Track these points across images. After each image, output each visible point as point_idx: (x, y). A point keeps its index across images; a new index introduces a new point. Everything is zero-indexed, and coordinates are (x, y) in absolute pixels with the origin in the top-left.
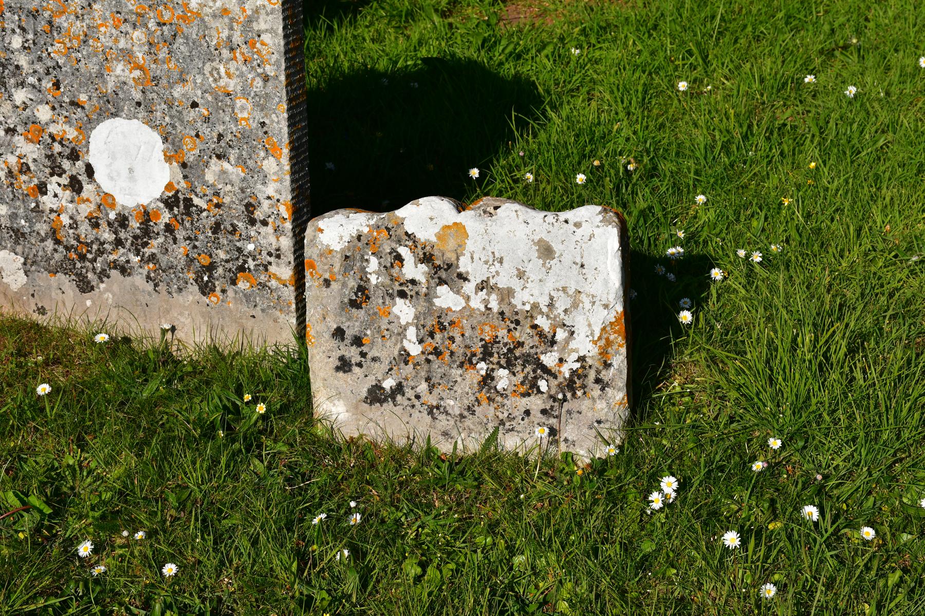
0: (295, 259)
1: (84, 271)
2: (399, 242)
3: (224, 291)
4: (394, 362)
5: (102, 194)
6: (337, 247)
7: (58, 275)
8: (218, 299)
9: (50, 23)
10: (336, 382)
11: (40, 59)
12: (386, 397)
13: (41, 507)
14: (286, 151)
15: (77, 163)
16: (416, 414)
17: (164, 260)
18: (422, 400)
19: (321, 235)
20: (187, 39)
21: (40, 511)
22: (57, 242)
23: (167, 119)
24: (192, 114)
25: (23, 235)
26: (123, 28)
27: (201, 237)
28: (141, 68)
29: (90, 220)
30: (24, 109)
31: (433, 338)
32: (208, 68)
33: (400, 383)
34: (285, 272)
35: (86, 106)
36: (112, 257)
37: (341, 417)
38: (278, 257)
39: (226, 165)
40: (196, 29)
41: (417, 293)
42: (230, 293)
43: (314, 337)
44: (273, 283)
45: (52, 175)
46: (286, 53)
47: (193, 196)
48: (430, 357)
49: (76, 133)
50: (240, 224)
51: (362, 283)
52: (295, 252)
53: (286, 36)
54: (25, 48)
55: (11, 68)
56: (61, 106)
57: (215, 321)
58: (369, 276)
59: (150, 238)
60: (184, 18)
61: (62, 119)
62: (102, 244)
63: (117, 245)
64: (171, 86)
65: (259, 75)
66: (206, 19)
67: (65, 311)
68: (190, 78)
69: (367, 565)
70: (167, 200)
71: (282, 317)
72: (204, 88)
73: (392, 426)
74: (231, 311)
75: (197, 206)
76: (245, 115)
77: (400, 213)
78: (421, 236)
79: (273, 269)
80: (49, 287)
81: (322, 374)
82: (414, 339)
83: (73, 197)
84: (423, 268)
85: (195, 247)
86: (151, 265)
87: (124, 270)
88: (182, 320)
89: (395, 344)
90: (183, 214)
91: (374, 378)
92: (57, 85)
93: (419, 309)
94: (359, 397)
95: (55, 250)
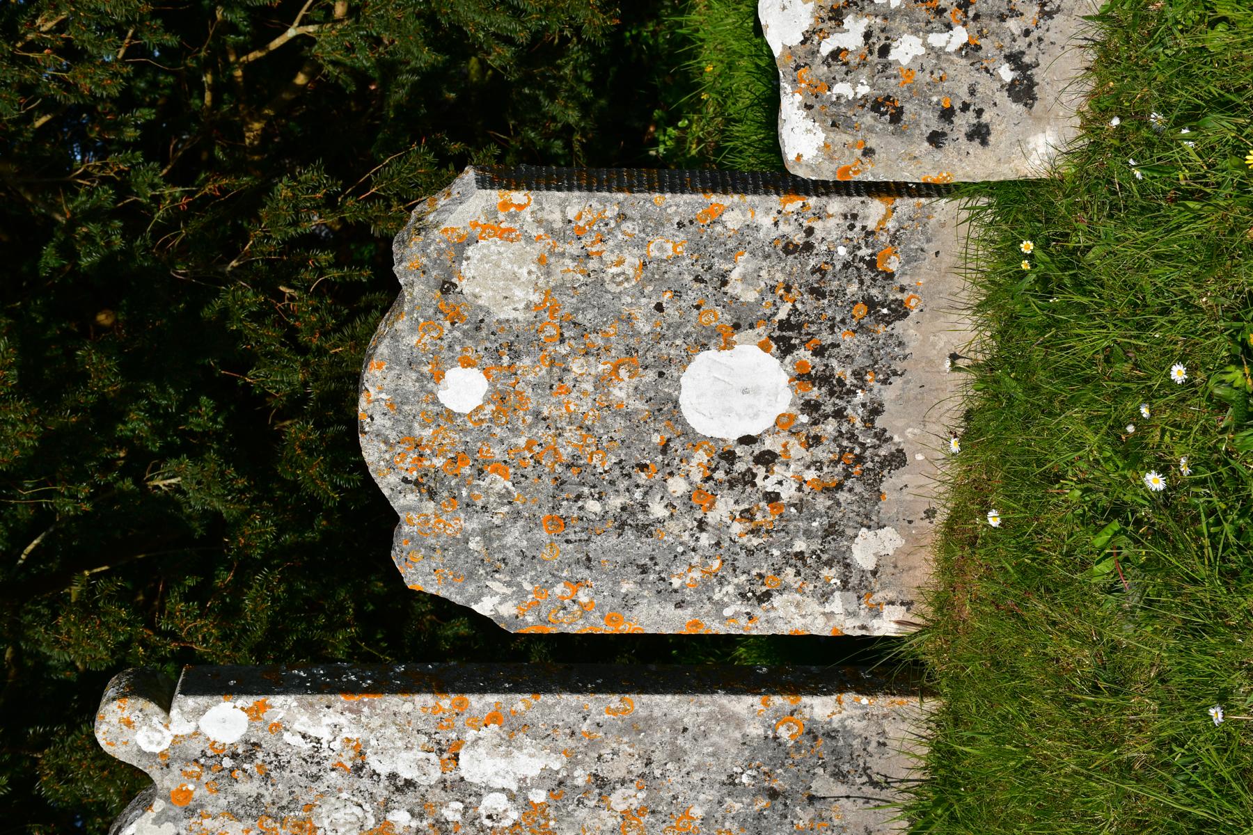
0: (859, 195)
1: (876, 459)
2: (814, 53)
3: (902, 289)
4: (977, 66)
5: (777, 428)
6: (820, 137)
7: (882, 490)
8: (912, 297)
9: (569, 466)
10: (1002, 146)
11: (612, 483)
12: (1025, 78)
13: (1111, 533)
14: (714, 198)
15: (738, 454)
16: (1051, 36)
17: (861, 361)
18: (1032, 27)
19: (805, 158)
20: (578, 309)
21: (1116, 534)
22: (840, 486)
23: (678, 342)
24: (671, 311)
25: (831, 525)
26: (569, 384)
27: (830, 313)
28: (616, 368)
29: (811, 446)
30: (674, 507)
31: (945, 10)
32: (612, 288)
33: (1006, 57)
34: (874, 210)
35: (667, 436)
36: (859, 424)
37: (1052, 141)
38: (855, 217)
39: (735, 275)
40: (565, 298)
41: (883, 30)
42: (905, 281)
43: (940, 173)
44: (891, 225)
45: (754, 485)
46: (590, 190)
47: (777, 319)
48: (971, 14)
49: (701, 452)
50: (812, 263)
51: (868, 105)
52: (849, 195)
53: (570, 189)
54: (600, 498)
55: (625, 516)
56: (668, 465)
57: (944, 303)
58: (859, 96)
59: (832, 375)
60: (553, 311)
61: (684, 466)
62: (841, 434)
63: (843, 417)
64: (636, 334)
65: (618, 226)
66: (552, 284)
67: (931, 486)
68: (626, 311)
69: (1206, 102)
70: (782, 352)
71: (938, 217)
72: (638, 294)
73: (1065, 69)
74: (929, 282)
75: (789, 315)
76: (669, 246)
77: (777, 51)
78: (806, 23)
79: (871, 225)
80: (898, 502)
81: (991, 164)
82: (946, 36)
83: (782, 463)
84: (849, 21)
85: (843, 321)
86: (868, 377)
87: (875, 410)
88: (942, 344)
89: (952, 62)
90: (800, 334)
91: (998, 94)
92: (643, 467)
93: (904, 28)
94: (1025, 115)
95: (850, 490)
